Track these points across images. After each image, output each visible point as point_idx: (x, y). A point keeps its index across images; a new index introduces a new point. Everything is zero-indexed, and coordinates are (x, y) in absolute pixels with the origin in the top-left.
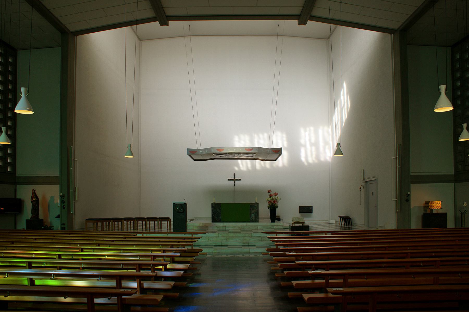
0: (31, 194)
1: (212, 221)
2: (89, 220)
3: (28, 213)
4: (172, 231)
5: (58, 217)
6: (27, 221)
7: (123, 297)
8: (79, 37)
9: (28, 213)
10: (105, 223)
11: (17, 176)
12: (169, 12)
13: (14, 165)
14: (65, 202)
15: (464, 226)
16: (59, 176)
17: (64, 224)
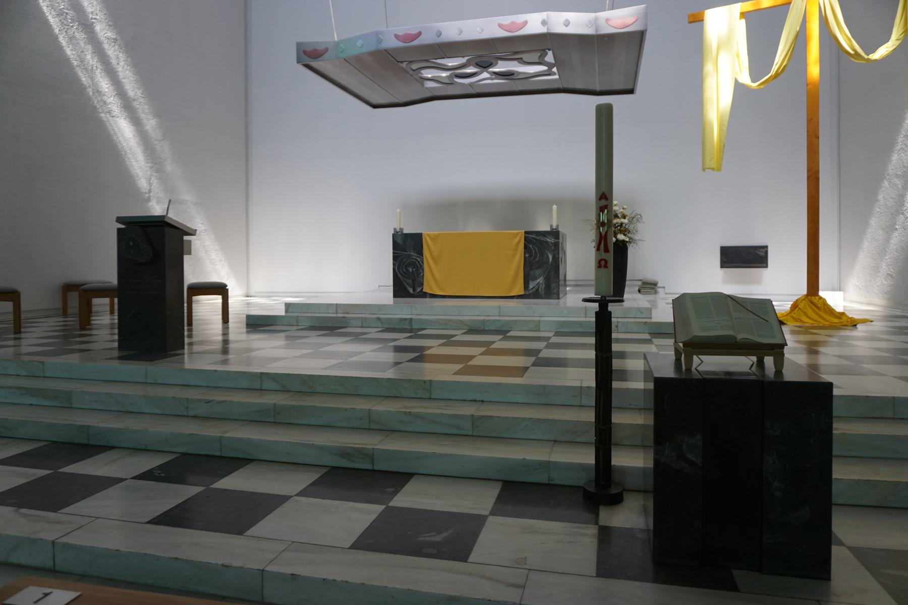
1: (395, 296)
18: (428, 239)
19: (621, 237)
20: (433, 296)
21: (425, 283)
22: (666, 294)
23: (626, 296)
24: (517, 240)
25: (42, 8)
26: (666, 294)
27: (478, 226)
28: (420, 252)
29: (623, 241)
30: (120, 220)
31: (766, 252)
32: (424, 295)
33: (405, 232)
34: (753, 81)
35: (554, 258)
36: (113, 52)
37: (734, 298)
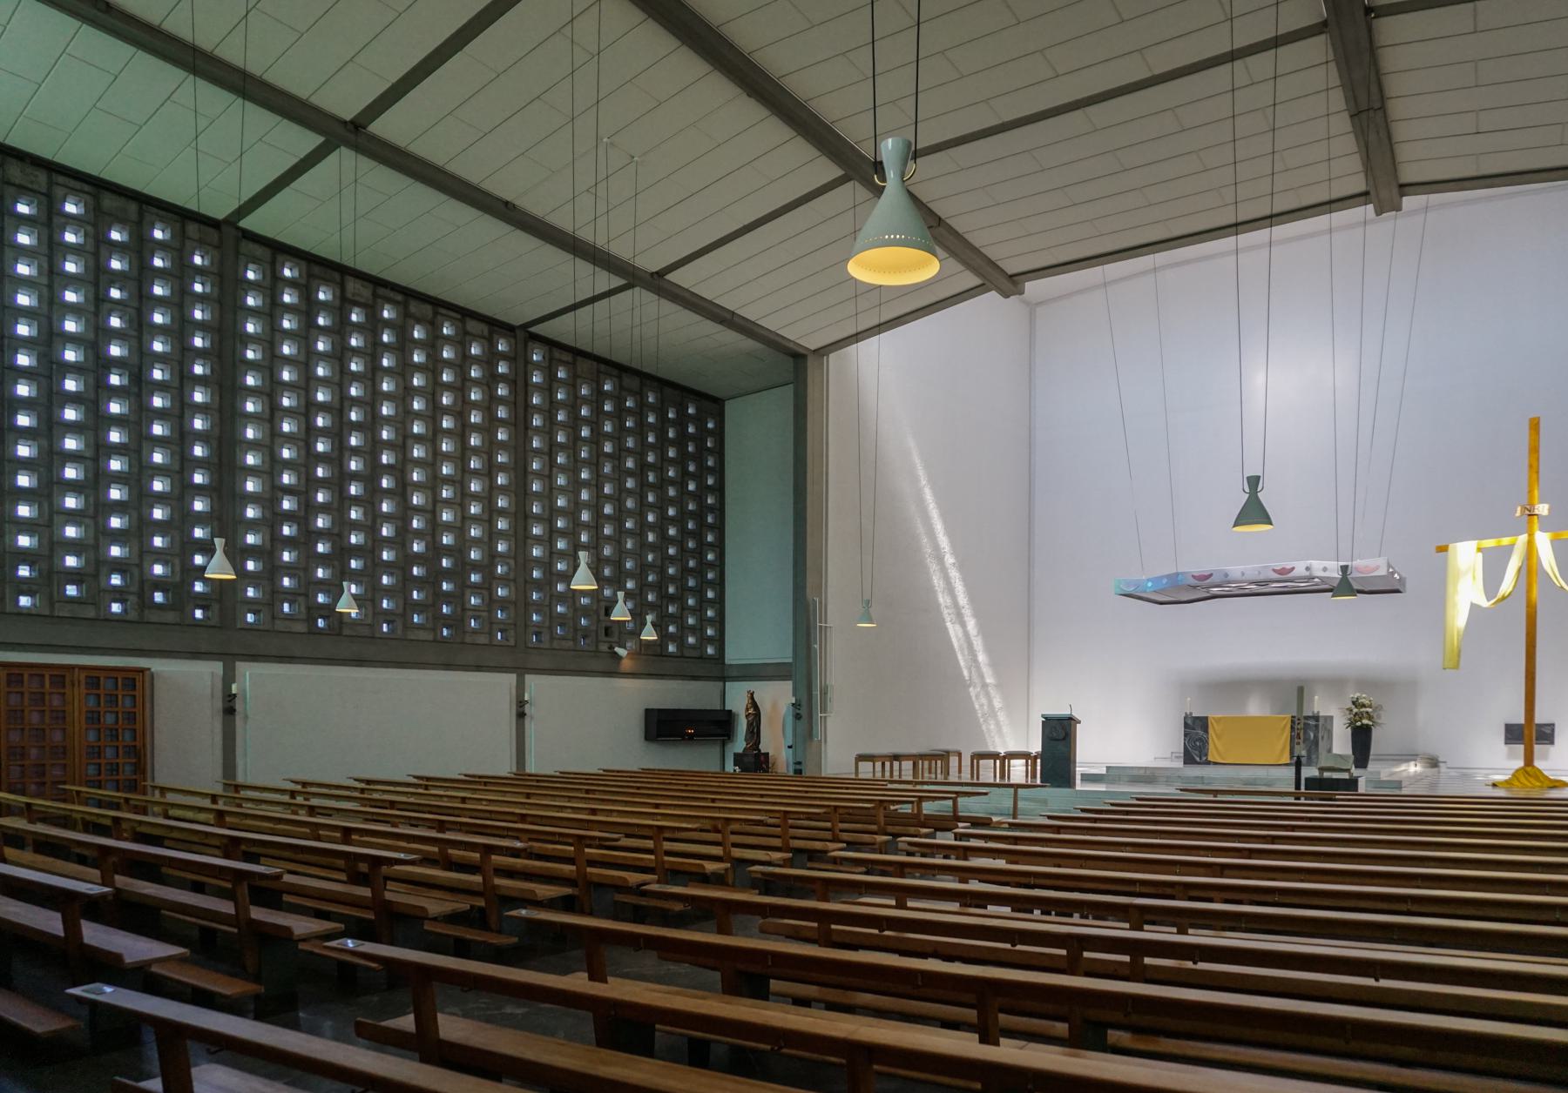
0: (745, 701)
1: (1185, 763)
2: (861, 758)
3: (739, 744)
4: (1038, 782)
5: (790, 747)
6: (736, 755)
7: (1147, 960)
8: (833, 357)
9: (739, 744)
10: (934, 762)
11: (727, 662)
12: (1012, 267)
13: (720, 641)
14: (801, 717)
15: (900, 776)
16: (790, 660)
17: (800, 763)
18: (1213, 721)
19: (1365, 721)
20: (1216, 763)
21: (1210, 753)
22: (1449, 768)
23: (1369, 766)
24: (1284, 722)
25: (188, 71)
26: (1449, 768)
27: (1255, 708)
28: (1206, 730)
29: (1367, 725)
30: (1043, 716)
31: (1553, 730)
32: (1208, 763)
33: (1194, 715)
34: (1488, 600)
35: (1315, 736)
36: (954, 574)
37: (1395, 762)
